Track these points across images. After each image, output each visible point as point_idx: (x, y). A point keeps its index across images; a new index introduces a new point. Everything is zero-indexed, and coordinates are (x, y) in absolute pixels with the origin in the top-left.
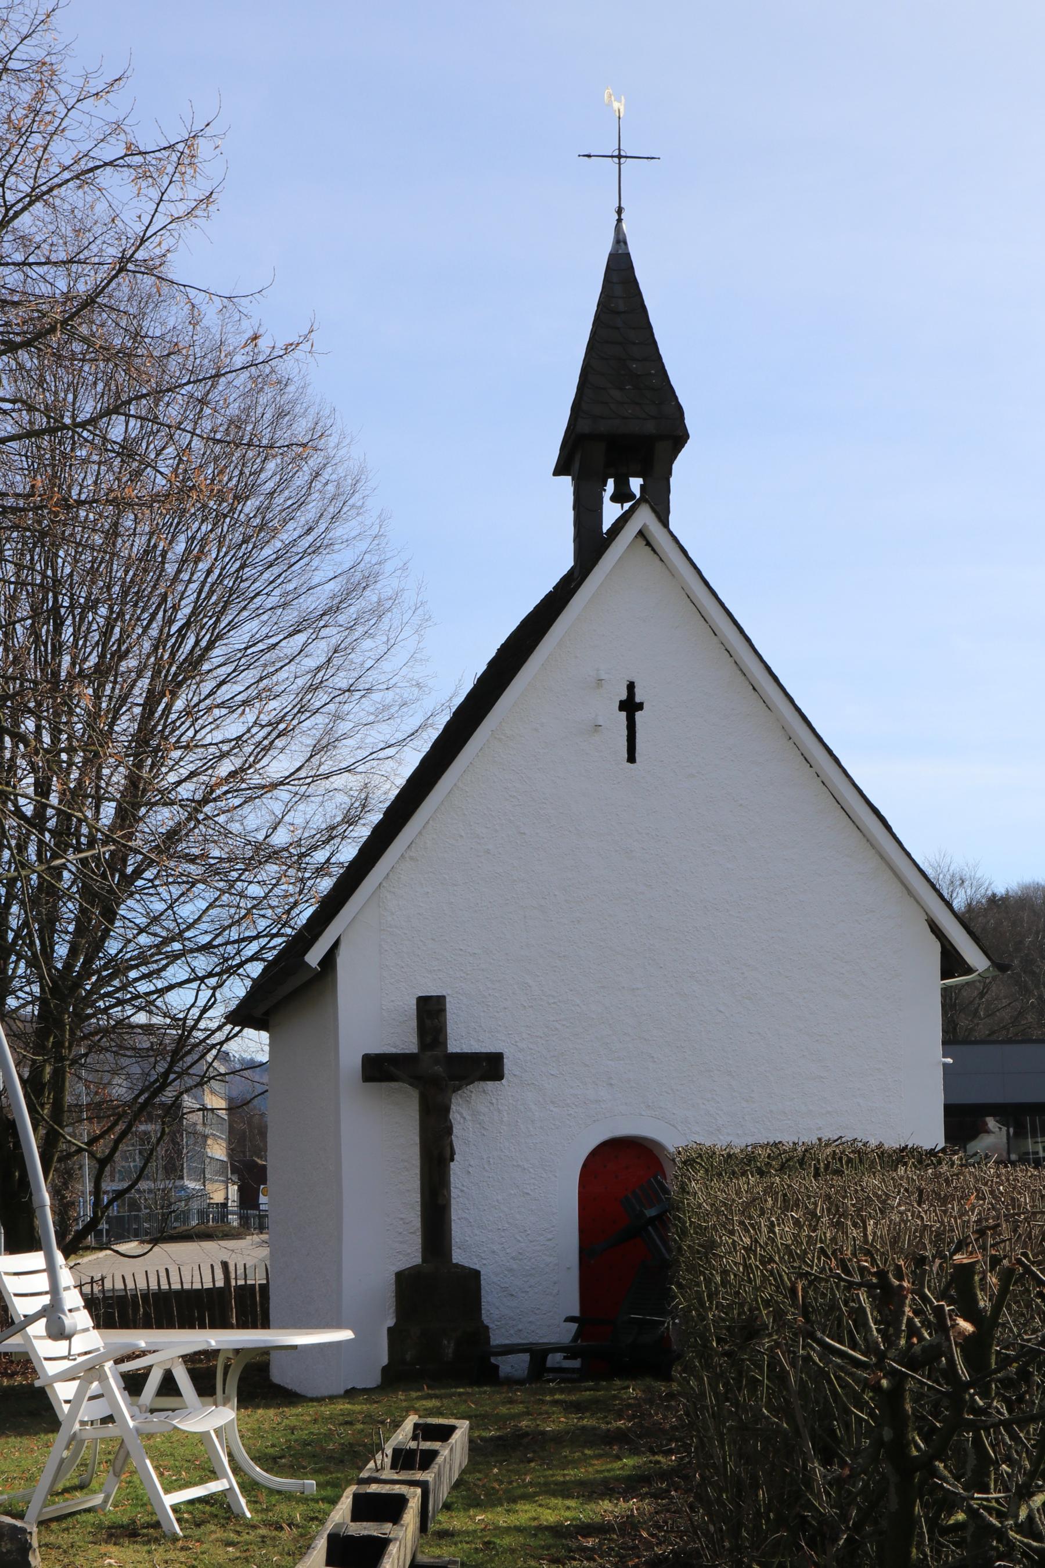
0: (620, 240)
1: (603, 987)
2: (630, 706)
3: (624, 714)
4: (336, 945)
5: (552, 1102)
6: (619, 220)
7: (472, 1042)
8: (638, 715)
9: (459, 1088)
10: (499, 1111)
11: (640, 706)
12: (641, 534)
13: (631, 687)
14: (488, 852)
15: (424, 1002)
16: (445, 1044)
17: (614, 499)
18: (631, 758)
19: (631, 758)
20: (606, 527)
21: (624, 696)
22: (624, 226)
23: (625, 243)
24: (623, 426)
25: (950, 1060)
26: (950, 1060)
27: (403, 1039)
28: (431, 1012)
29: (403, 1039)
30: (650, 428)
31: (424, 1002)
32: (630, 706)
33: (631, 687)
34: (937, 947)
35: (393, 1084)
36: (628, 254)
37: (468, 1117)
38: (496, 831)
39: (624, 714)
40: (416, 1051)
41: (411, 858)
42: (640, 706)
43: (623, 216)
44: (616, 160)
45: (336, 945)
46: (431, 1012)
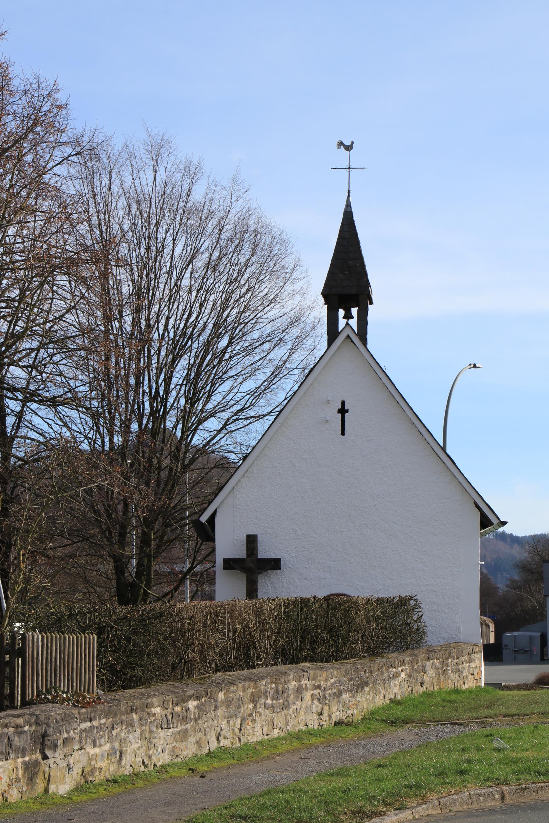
0: (348, 205)
1: (328, 531)
2: (343, 411)
3: (340, 414)
4: (215, 512)
5: (305, 579)
6: (349, 196)
7: (272, 554)
8: (346, 415)
9: (261, 573)
10: (283, 582)
11: (347, 411)
12: (348, 336)
13: (343, 403)
14: (280, 474)
15: (248, 536)
16: (257, 555)
17: (344, 318)
18: (343, 433)
19: (343, 433)
20: (339, 331)
21: (340, 407)
22: (351, 198)
23: (351, 206)
24: (348, 285)
25: (483, 563)
26: (483, 563)
27: (240, 552)
28: (252, 540)
29: (240, 552)
30: (354, 291)
31: (248, 536)
32: (343, 411)
33: (343, 403)
34: (478, 514)
35: (234, 571)
36: (352, 212)
37: (269, 585)
38: (283, 465)
39: (340, 414)
40: (245, 556)
41: (247, 477)
42: (347, 411)
43: (350, 194)
44: (348, 170)
45: (215, 512)
46: (252, 540)
